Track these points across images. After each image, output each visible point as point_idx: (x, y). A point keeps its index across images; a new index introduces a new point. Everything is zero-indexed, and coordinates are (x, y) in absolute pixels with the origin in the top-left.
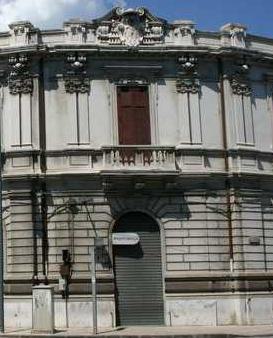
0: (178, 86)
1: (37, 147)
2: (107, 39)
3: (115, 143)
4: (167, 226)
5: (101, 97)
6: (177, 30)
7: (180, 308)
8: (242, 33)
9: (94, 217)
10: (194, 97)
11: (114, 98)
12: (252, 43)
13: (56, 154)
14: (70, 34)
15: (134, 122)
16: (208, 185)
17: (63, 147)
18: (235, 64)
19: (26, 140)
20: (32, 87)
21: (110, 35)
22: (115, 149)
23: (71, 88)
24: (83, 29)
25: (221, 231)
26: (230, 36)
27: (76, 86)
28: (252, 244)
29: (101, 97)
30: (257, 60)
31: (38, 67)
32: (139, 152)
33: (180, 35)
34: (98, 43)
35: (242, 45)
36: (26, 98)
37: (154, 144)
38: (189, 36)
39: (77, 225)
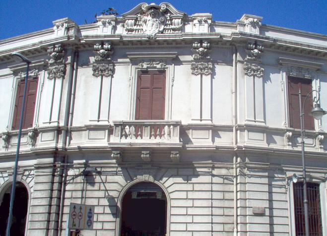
0: (193, 69)
1: (62, 124)
2: (132, 30)
3: (133, 120)
4: (167, 185)
5: (124, 76)
6: (196, 22)
7: (57, 70)
8: (257, 23)
9: (108, 186)
10: (207, 79)
11: (134, 82)
12: (266, 33)
13: (79, 129)
14: (101, 27)
15: (150, 96)
16: (218, 156)
17: (107, 179)
18: (248, 49)
19: (55, 118)
20: (64, 72)
21: (135, 27)
22: (130, 124)
23: (98, 72)
24: (113, 23)
25: (226, 202)
26: (245, 25)
27: (102, 71)
28: (256, 215)
29: (124, 76)
30: (271, 46)
31: (47, 234)
32: (146, 126)
33: (198, 25)
34: (125, 33)
35: (256, 32)
36: (59, 82)
37: (167, 118)
38: (206, 25)
39: (89, 194)
